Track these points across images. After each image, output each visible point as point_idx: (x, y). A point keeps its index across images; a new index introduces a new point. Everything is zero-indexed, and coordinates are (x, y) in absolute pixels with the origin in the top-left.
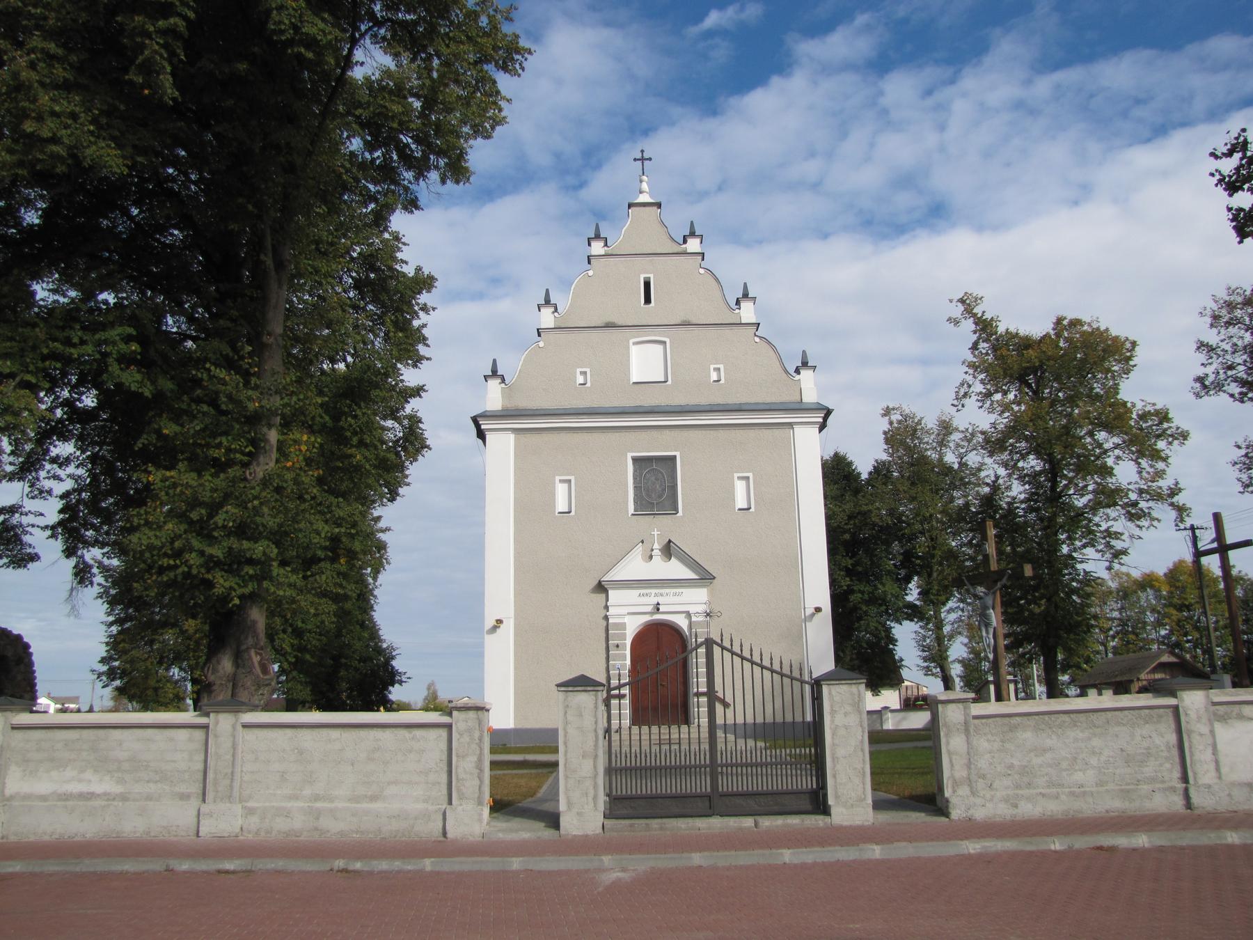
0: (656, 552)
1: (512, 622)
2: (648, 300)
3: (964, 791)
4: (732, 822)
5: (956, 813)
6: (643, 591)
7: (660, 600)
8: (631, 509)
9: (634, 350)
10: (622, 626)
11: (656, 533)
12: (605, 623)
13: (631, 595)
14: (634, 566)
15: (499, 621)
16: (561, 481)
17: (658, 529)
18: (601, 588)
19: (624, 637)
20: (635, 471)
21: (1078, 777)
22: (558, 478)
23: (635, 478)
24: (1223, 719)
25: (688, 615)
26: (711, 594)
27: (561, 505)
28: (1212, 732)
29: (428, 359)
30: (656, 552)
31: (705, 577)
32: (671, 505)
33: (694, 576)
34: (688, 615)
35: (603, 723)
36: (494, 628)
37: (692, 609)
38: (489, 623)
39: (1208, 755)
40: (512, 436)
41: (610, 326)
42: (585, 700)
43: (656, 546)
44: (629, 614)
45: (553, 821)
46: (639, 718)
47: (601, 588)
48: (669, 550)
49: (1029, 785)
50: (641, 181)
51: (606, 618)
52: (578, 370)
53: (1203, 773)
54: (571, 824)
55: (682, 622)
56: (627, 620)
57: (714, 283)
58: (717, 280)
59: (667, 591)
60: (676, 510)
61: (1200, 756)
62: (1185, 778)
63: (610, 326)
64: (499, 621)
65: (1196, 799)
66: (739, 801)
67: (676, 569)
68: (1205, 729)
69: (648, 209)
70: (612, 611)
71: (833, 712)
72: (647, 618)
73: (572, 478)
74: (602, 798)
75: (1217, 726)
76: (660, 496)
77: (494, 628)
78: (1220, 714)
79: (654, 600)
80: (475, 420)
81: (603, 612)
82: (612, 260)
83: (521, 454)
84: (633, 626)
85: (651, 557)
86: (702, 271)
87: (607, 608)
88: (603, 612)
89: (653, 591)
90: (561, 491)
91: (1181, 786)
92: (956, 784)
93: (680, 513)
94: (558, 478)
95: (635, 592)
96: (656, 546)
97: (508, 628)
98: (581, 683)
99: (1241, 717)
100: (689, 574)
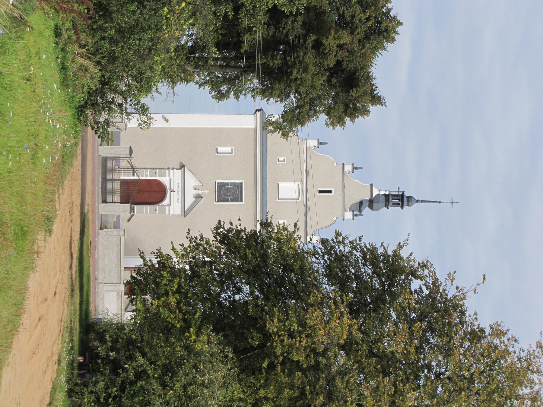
0: (198, 192)
1: (168, 126)
2: (321, 192)
3: (105, 234)
4: (100, 183)
5: (100, 231)
6: (180, 185)
7: (176, 193)
8: (218, 181)
9: (296, 184)
10: (165, 176)
11: (207, 192)
12: (166, 168)
13: (178, 180)
14: (191, 181)
15: (168, 121)
16: (232, 149)
17: (209, 193)
18: (182, 166)
19: (160, 176)
20: (236, 183)
21: (107, 260)
22: (233, 148)
23: (233, 183)
24: (118, 294)
25: (169, 205)
26: (178, 216)
27: (221, 149)
28: (115, 291)
29: (254, 101)
30: (198, 192)
31: (185, 213)
32: (220, 199)
33: (186, 209)
34: (169, 205)
35: (121, 156)
36: (165, 119)
37: (171, 207)
38: (167, 116)
39: (110, 289)
40: (253, 126)
41: (307, 172)
42: (128, 152)
43: (201, 192)
44: (170, 179)
45: (101, 145)
46: (125, 183)
47: (182, 166)
48: (198, 197)
49: (105, 249)
50: (386, 191)
51: (168, 169)
52: (285, 158)
53: (107, 288)
54: (101, 148)
55: (166, 202)
56: (168, 178)
57: (328, 224)
58: (330, 225)
59: (180, 196)
60: (218, 201)
61: (110, 288)
62: (105, 284)
63: (307, 172)
64: (168, 121)
65: (101, 284)
66: (105, 185)
67: (190, 200)
68: (116, 289)
69: (369, 193)
70: (172, 171)
71: (123, 206)
72: (168, 187)
73: (233, 154)
74: (106, 155)
75: (116, 293)
76: (224, 195)
77: (165, 119)
78: (119, 294)
79: (176, 190)
80: (261, 110)
81: (171, 167)
82: (342, 175)
83: (245, 130)
84: (165, 180)
85: (196, 189)
86: (335, 218)
87: (173, 169)
88: (171, 167)
89: (180, 190)
90: (228, 149)
91: (104, 282)
92: (107, 232)
93: (215, 203)
94: (233, 148)
95: (180, 182)
96: (201, 192)
97: (165, 125)
98: (131, 152)
99: (118, 298)
100: (187, 206)
